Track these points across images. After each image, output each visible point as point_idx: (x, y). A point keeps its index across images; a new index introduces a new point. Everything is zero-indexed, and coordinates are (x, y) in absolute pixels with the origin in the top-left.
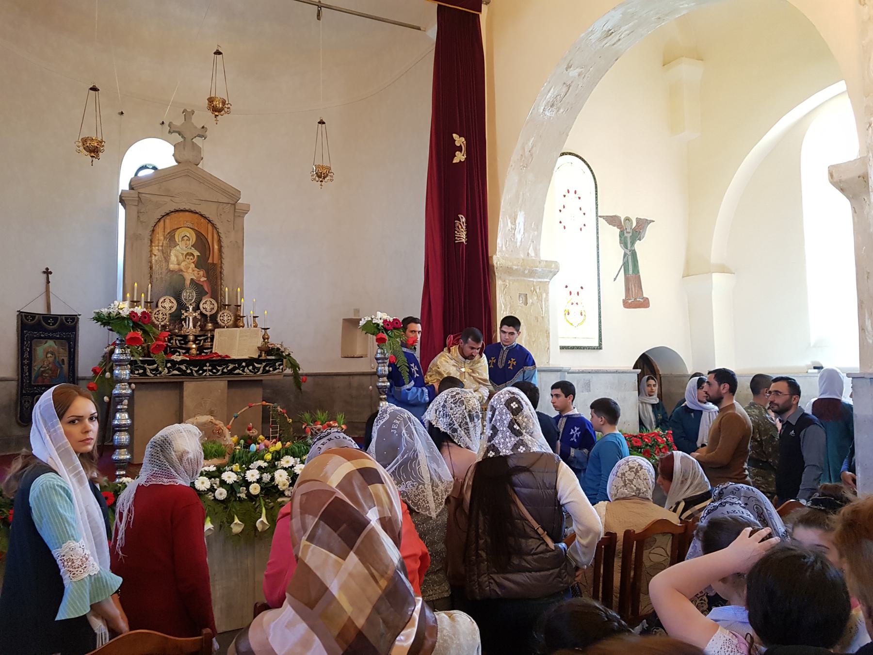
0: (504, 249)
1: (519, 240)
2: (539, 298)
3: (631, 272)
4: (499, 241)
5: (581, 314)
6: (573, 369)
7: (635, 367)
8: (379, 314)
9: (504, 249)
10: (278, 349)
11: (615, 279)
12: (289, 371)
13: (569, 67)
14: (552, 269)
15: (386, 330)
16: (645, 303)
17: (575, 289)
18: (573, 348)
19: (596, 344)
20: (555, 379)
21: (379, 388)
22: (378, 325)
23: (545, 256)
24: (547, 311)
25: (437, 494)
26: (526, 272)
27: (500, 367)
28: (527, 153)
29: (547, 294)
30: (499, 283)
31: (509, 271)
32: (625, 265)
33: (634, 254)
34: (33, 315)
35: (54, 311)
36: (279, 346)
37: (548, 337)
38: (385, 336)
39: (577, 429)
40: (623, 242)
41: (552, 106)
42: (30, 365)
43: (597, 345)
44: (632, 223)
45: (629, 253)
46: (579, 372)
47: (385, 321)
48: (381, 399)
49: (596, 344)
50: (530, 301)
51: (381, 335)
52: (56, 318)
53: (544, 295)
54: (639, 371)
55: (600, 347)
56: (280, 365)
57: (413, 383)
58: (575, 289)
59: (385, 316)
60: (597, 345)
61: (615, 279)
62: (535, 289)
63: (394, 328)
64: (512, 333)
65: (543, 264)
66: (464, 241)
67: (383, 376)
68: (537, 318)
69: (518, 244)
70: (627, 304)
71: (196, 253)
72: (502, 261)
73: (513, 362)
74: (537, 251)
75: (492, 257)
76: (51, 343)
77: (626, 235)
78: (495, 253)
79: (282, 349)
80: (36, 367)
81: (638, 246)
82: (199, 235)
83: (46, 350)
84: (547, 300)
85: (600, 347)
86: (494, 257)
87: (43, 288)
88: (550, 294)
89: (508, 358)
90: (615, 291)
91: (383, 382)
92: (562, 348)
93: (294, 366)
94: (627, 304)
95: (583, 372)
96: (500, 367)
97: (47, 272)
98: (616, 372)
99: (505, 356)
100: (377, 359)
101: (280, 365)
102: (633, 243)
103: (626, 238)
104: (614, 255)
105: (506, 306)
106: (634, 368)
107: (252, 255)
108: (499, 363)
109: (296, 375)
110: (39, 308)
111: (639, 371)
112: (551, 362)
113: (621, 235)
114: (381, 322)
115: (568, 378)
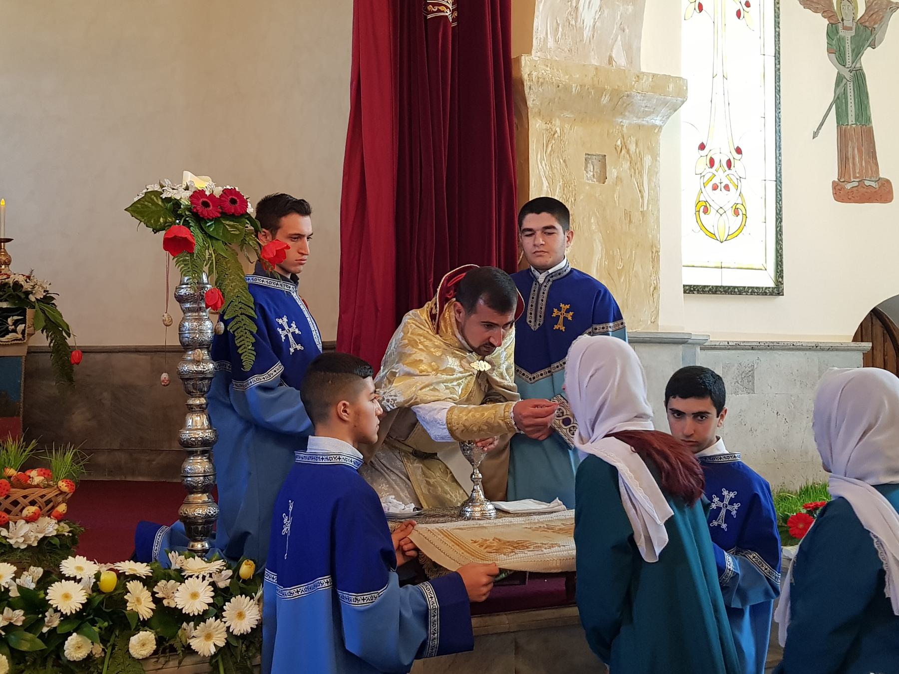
0: (551, 43)
1: (589, 23)
2: (636, 165)
3: (852, 119)
4: (538, 23)
5: (736, 213)
6: (715, 339)
7: (860, 336)
8: (189, 177)
9: (551, 43)
10: (17, 285)
11: (815, 135)
12: (42, 340)
14: (669, 93)
15: (199, 219)
16: (882, 193)
17: (721, 151)
18: (715, 290)
19: (767, 280)
20: (670, 364)
21: (185, 378)
22: (177, 203)
23: (648, 64)
24: (655, 200)
26: (605, 100)
27: (534, 326)
29: (655, 157)
30: (536, 126)
32: (840, 102)
33: (859, 78)
36: (21, 280)
37: (655, 259)
38: (198, 238)
39: (728, 495)
40: (836, 50)
43: (771, 284)
44: (856, 8)
45: (848, 75)
46: (729, 347)
47: (198, 194)
48: (191, 409)
49: (767, 280)
50: (612, 173)
51: (179, 229)
53: (648, 160)
54: (868, 345)
55: (777, 291)
56: (16, 323)
57: (277, 370)
58: (721, 158)
59: (203, 183)
60: (771, 284)
61: (815, 135)
62: (624, 145)
63: (226, 215)
64: (701, 416)
65: (646, 83)
66: (448, 13)
67: (201, 345)
68: (628, 215)
69: (587, 33)
70: (841, 193)
72: (544, 71)
73: (564, 312)
74: (632, 52)
75: (518, 60)
77: (842, 33)
78: (529, 52)
79: (27, 286)
81: (869, 60)
84: (654, 171)
85: (777, 291)
86: (525, 60)
88: (661, 159)
89: (552, 303)
90: (817, 160)
91: (197, 362)
92: (690, 290)
93: (55, 327)
94: (841, 193)
95: (737, 347)
96: (534, 326)
98: (816, 348)
99: (544, 297)
100: (181, 299)
101: (16, 323)
102: (857, 53)
103: (841, 40)
104: (815, 78)
106: (855, 339)
108: (530, 319)
109: (60, 349)
111: (868, 345)
112: (660, 322)
113: (832, 32)
114: (183, 197)
115: (702, 360)
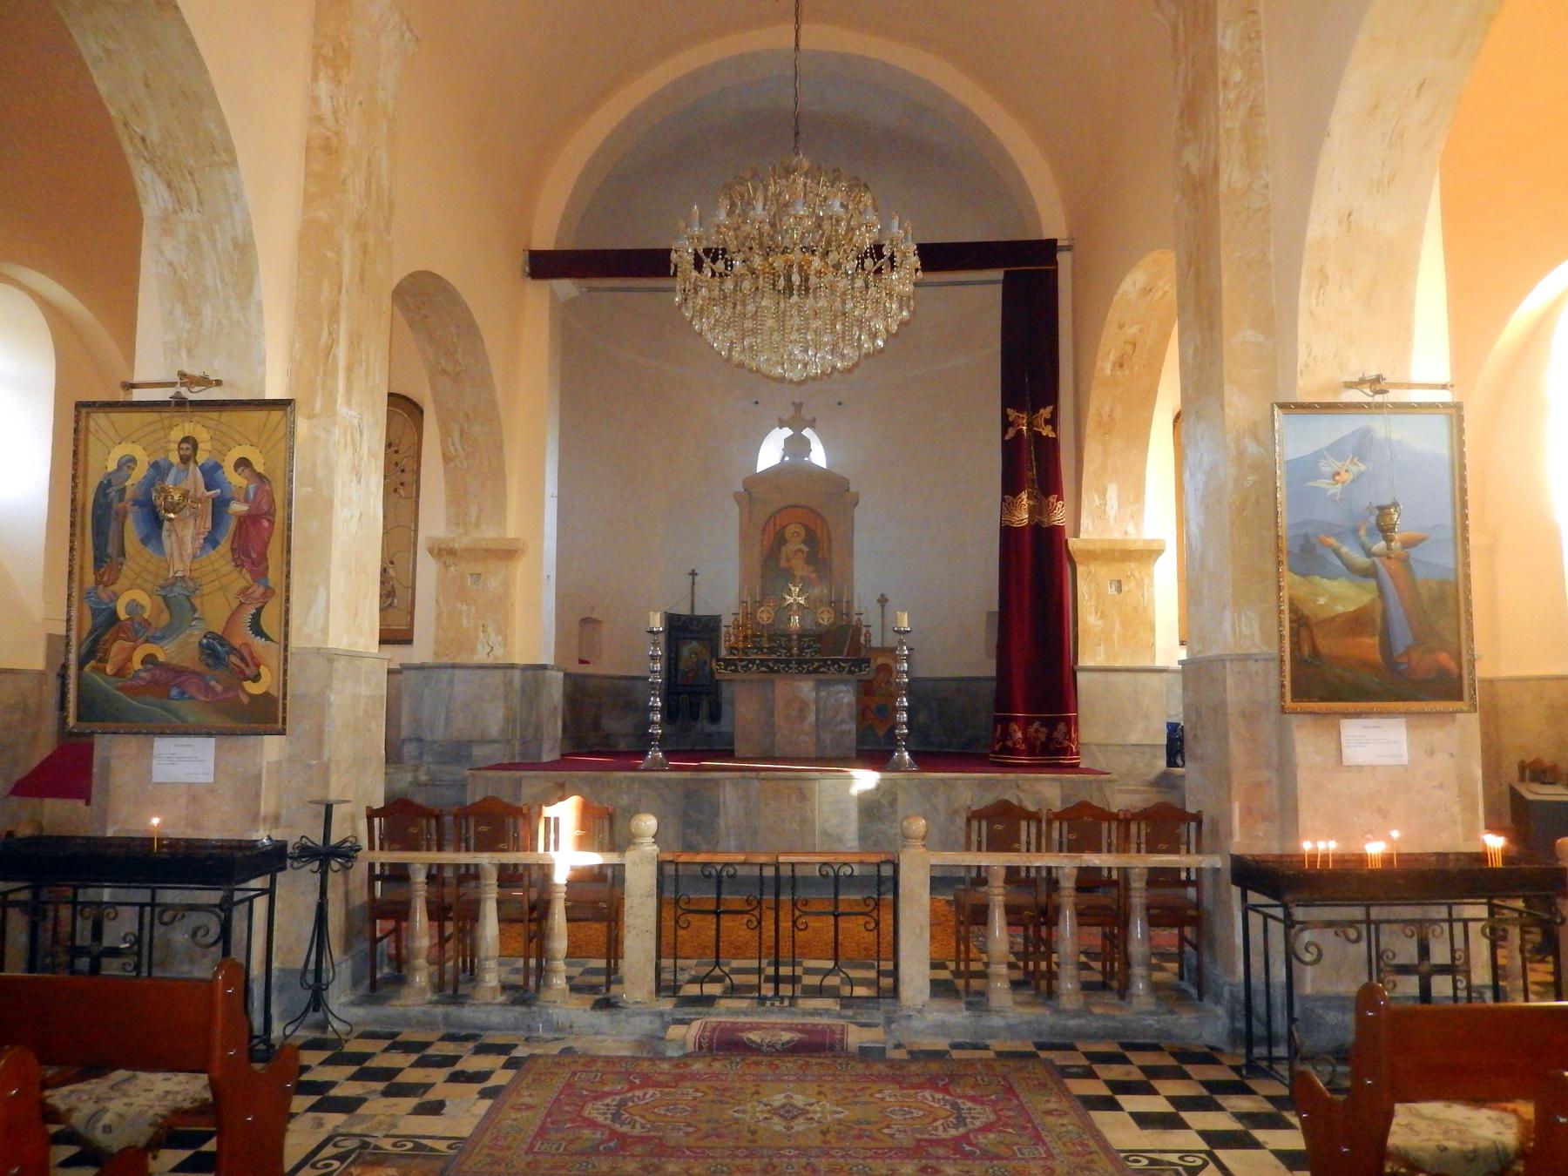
2: (1140, 584)
13: (1121, 326)
25: (194, 241)
28: (1106, 418)
31: (1092, 555)
34: (679, 616)
35: (699, 612)
41: (1121, 366)
42: (676, 665)
50: (1125, 588)
52: (699, 618)
53: (1146, 581)
68: (1135, 609)
71: (806, 549)
76: (694, 643)
80: (682, 666)
82: (807, 529)
83: (690, 650)
87: (689, 591)
97: (693, 574)
105: (1090, 595)
107: (862, 541)
110: (683, 610)
